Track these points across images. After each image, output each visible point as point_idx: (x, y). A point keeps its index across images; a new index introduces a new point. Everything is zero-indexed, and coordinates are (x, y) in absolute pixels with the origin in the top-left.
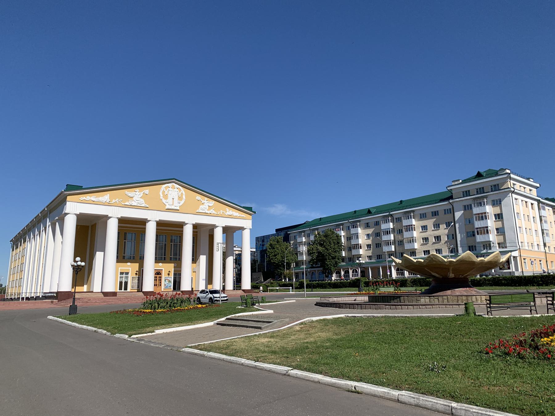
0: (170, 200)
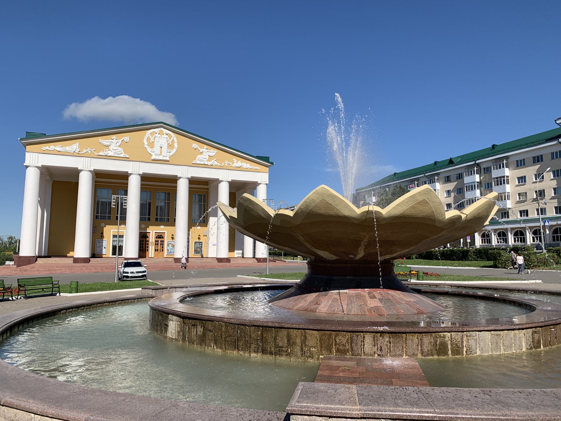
0: (157, 149)
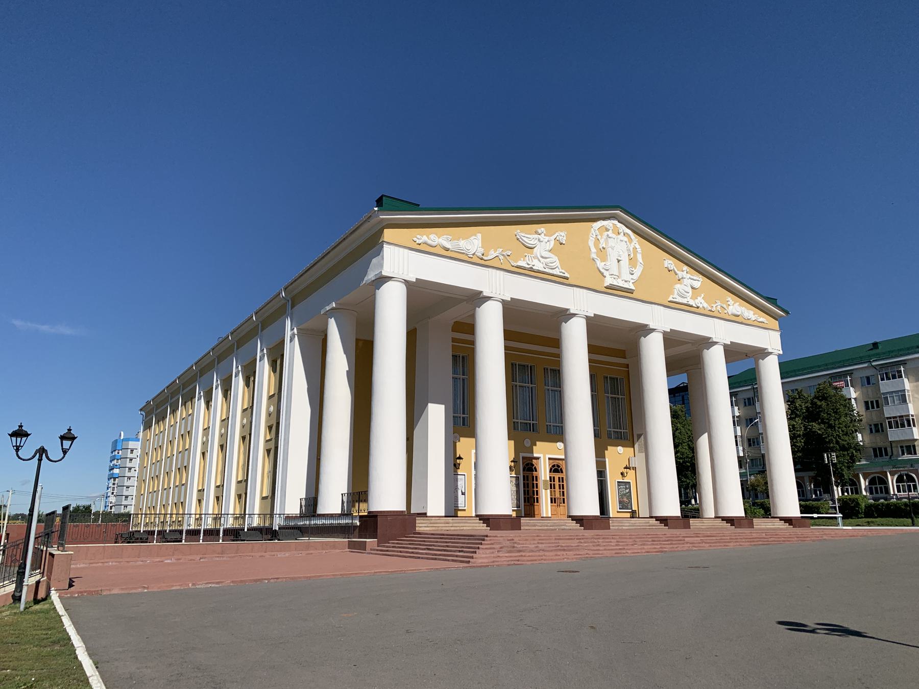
0: (612, 264)
